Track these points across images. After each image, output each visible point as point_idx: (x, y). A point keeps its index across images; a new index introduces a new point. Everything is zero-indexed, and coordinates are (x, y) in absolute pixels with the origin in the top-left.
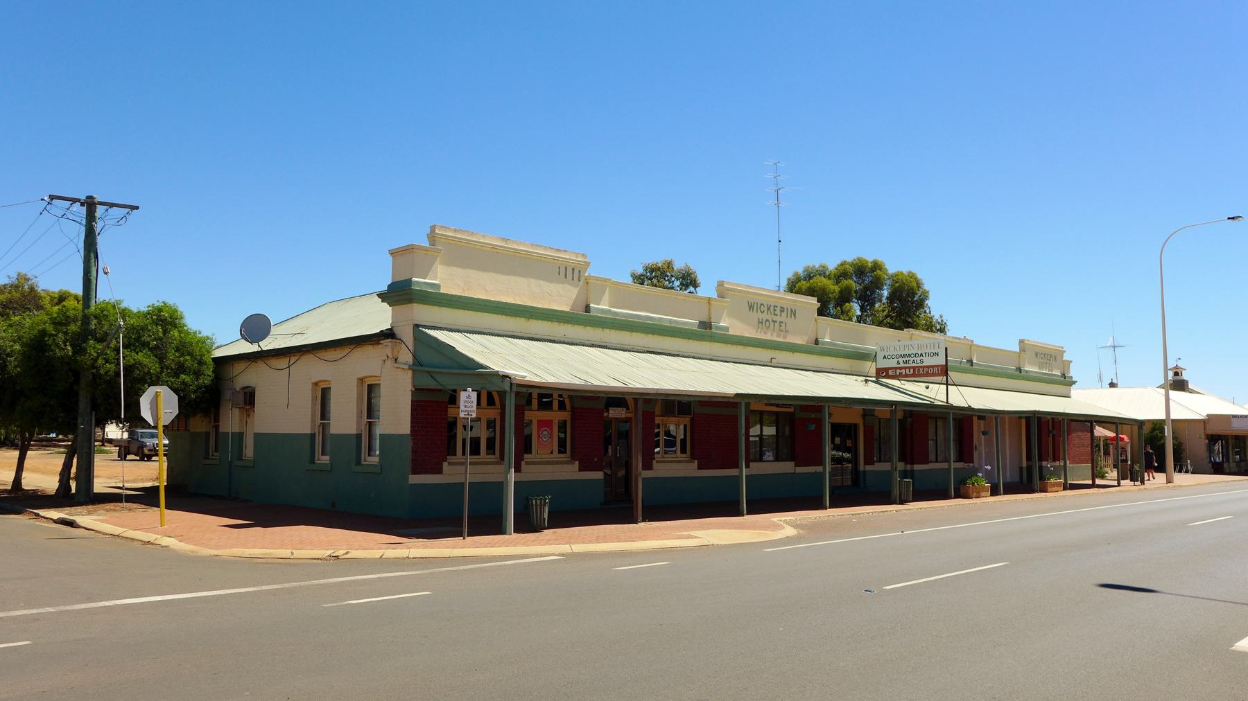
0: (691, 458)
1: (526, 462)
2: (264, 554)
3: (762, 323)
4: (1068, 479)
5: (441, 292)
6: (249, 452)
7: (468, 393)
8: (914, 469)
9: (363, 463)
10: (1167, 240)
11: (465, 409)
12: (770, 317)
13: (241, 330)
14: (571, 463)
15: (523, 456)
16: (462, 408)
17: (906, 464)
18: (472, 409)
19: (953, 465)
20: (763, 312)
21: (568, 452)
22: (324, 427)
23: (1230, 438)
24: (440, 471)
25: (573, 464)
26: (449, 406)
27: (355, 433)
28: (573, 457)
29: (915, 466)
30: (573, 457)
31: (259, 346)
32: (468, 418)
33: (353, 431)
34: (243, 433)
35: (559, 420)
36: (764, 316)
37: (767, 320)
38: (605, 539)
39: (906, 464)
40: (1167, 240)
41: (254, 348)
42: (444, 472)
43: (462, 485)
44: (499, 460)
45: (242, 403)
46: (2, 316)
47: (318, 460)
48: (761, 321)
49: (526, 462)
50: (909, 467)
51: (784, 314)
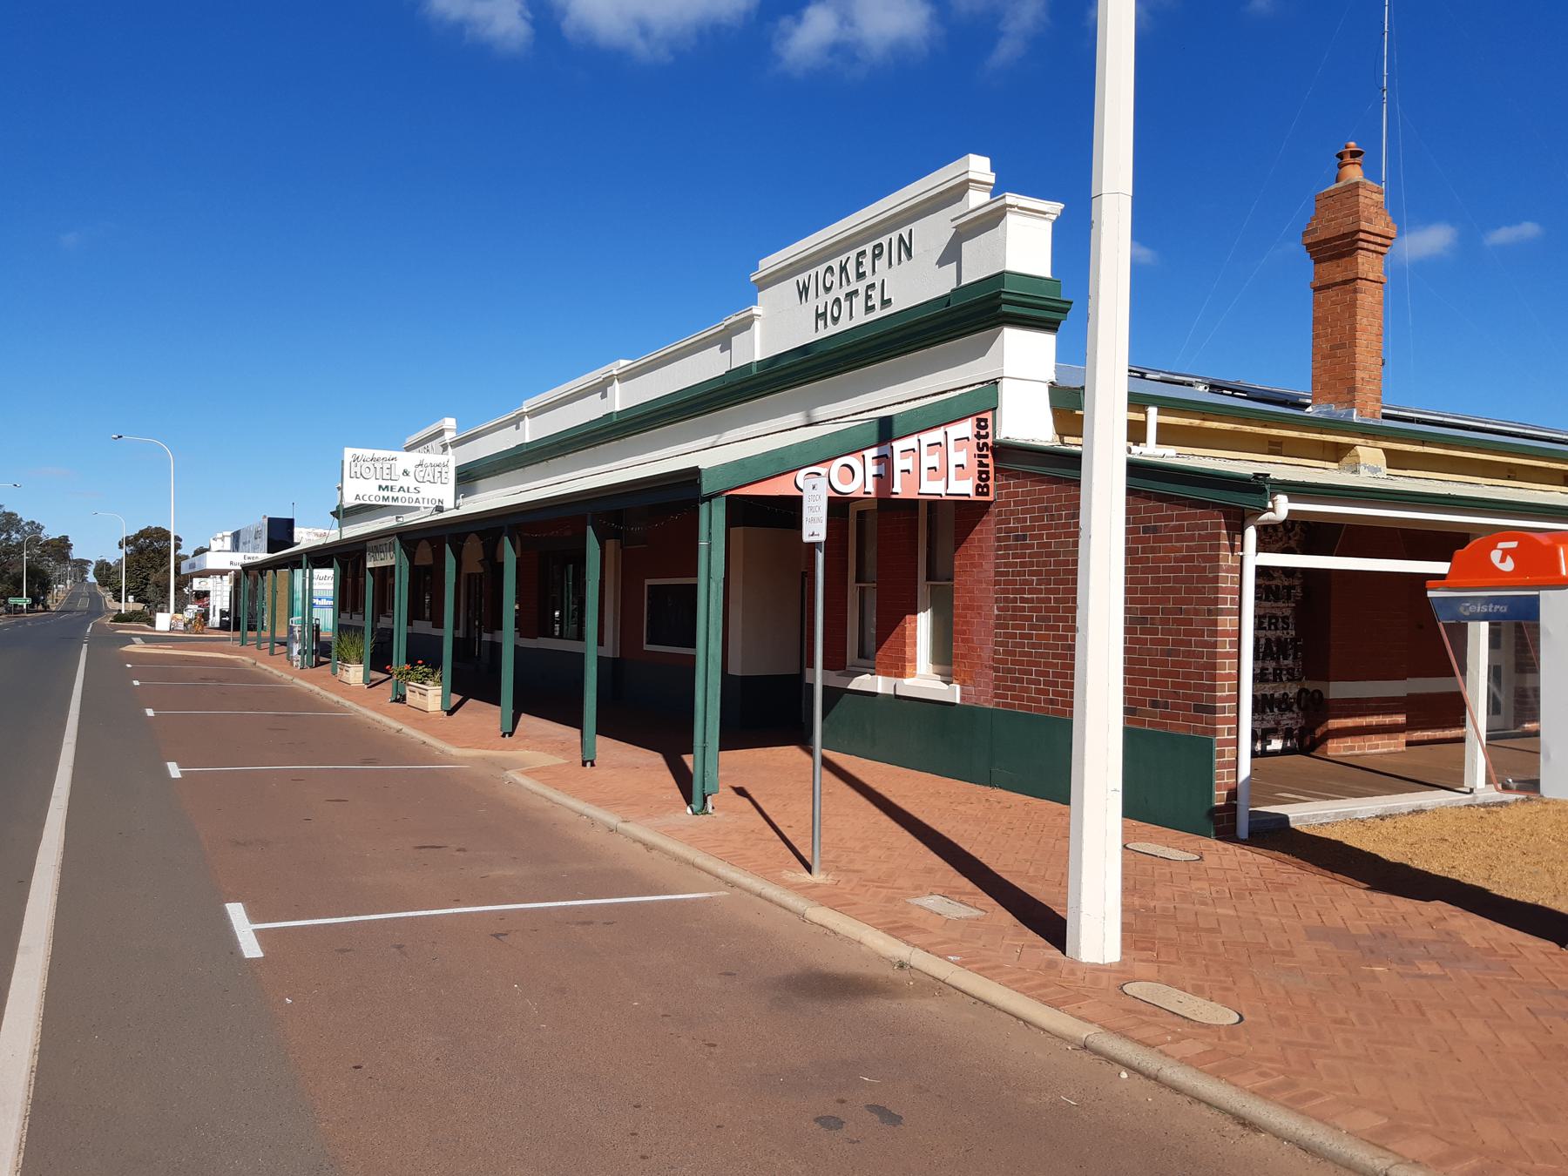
10: (790, 430)
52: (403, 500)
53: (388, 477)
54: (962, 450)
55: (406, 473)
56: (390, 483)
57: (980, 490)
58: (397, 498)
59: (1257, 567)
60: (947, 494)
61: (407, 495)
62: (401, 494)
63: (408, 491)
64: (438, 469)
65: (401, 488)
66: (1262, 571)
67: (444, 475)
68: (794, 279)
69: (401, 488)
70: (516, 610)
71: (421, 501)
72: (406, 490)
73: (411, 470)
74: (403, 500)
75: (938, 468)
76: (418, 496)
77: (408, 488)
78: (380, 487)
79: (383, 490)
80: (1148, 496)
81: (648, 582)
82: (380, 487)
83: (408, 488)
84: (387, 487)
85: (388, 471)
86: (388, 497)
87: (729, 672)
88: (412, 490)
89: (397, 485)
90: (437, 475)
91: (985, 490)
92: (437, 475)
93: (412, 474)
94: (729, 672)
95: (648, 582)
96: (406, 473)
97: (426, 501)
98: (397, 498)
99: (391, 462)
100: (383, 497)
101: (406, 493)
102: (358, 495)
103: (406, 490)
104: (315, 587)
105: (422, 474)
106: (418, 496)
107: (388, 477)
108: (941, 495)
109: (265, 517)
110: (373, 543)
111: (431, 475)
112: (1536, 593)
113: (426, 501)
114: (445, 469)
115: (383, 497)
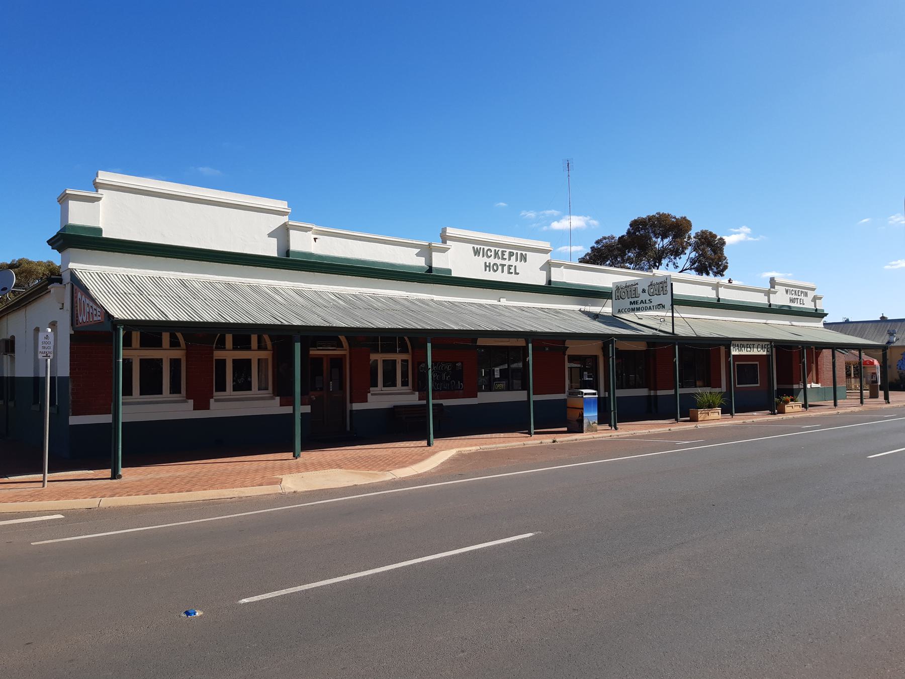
1: (215, 399)
2: (509, 442)
3: (489, 266)
4: (808, 400)
5: (453, 275)
11: (43, 350)
12: (499, 262)
14: (272, 398)
15: (369, 389)
18: (50, 350)
19: (431, 402)
25: (274, 399)
26: (311, 348)
28: (189, 397)
30: (189, 397)
35: (132, 359)
37: (495, 264)
38: (189, 485)
39: (650, 390)
42: (369, 401)
46: (1, 302)
48: (487, 264)
49: (215, 399)
50: (652, 393)
51: (513, 258)
53: (634, 296)
55: (644, 291)
56: (635, 299)
58: (639, 308)
62: (642, 305)
63: (646, 303)
68: (474, 245)
72: (644, 302)
73: (647, 288)
77: (645, 300)
78: (631, 302)
80: (125, 349)
81: (758, 385)
82: (631, 302)
83: (645, 300)
84: (634, 302)
88: (647, 302)
89: (639, 299)
90: (661, 289)
92: (661, 289)
93: (647, 291)
95: (758, 385)
98: (639, 308)
99: (635, 287)
100: (632, 308)
102: (619, 310)
103: (644, 302)
104: (833, 401)
105: (652, 290)
107: (634, 296)
109: (883, 314)
110: (737, 343)
111: (657, 291)
112: (214, 361)
114: (665, 285)
115: (632, 308)
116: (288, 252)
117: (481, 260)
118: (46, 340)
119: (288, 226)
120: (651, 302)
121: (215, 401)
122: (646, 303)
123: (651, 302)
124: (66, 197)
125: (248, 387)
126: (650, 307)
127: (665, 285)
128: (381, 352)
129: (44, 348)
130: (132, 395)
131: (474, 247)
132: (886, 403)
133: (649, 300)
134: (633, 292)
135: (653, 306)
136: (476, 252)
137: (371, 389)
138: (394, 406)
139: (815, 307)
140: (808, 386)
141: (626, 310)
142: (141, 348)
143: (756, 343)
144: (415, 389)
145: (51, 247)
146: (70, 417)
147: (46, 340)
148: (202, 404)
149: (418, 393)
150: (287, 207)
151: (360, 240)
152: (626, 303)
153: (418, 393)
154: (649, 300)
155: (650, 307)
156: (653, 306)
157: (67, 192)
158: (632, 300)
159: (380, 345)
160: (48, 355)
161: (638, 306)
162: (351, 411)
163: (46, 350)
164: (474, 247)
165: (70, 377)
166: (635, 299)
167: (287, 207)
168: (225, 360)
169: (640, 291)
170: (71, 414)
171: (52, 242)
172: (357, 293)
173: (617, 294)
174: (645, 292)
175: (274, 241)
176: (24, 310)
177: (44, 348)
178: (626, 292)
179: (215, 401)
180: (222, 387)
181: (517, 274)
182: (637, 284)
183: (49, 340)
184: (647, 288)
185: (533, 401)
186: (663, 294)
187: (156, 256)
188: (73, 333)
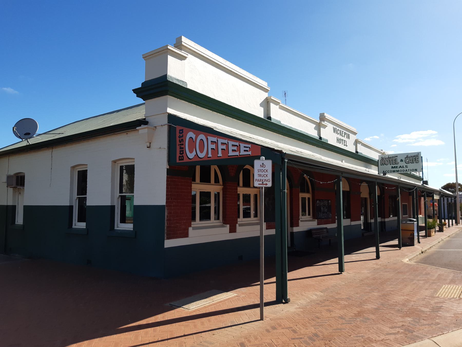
0: (313, 218)
6: (20, 220)
7: (263, 162)
8: (386, 221)
9: (116, 228)
10: (456, 117)
11: (259, 178)
13: (13, 128)
16: (256, 177)
17: (382, 218)
18: (266, 178)
20: (338, 134)
21: (311, 215)
22: (82, 201)
23: (200, 206)
24: (186, 235)
26: (193, 182)
27: (69, 205)
29: (386, 219)
31: (28, 142)
32: (262, 188)
33: (108, 203)
34: (15, 206)
36: (340, 137)
40: (456, 117)
41: (24, 143)
43: (13, 208)
44: (222, 224)
45: (14, 185)
47: (75, 225)
49: (239, 224)
50: (383, 220)
52: (401, 171)
53: (395, 163)
54: (214, 144)
55: (402, 161)
56: (396, 165)
57: (180, 158)
58: (399, 170)
59: (211, 192)
60: (240, 155)
61: (402, 169)
62: (400, 169)
63: (403, 167)
64: (414, 158)
65: (400, 167)
66: (201, 219)
67: (417, 160)
69: (400, 167)
70: (254, 213)
71: (408, 170)
72: (402, 167)
73: (404, 159)
74: (401, 171)
75: (225, 149)
76: (407, 169)
77: (403, 166)
79: (393, 168)
83: (403, 166)
84: (395, 167)
85: (394, 161)
86: (395, 170)
87: (275, 299)
88: (404, 167)
90: (414, 160)
91: (182, 158)
92: (414, 160)
93: (404, 161)
94: (275, 299)
96: (402, 161)
97: (410, 170)
98: (399, 170)
99: (395, 158)
100: (393, 171)
101: (402, 168)
102: (384, 171)
103: (402, 167)
105: (408, 160)
106: (407, 169)
108: (238, 155)
113: (410, 170)
115: (393, 171)
116: (269, 118)
117: (336, 136)
118: (261, 168)
119: (270, 100)
120: (407, 167)
121: (193, 229)
122: (403, 167)
123: (407, 167)
124: (165, 51)
125: (208, 218)
126: (406, 170)
127: (417, 158)
128: (307, 193)
129: (260, 175)
130: (243, 218)
131: (333, 127)
132: (456, 225)
133: (406, 166)
134: (394, 161)
135: (409, 170)
136: (335, 130)
137: (192, 223)
138: (310, 229)
139: (419, 175)
140: (419, 216)
141: (389, 172)
142: (201, 183)
143: (217, 206)
144: (225, 222)
145: (136, 95)
146: (165, 240)
147: (261, 168)
148: (233, 230)
149: (316, 220)
150: (267, 86)
151: (293, 114)
152: (389, 167)
153: (316, 220)
154: (406, 166)
155: (406, 170)
156: (409, 170)
157: (169, 47)
158: (393, 166)
159: (286, 190)
160: (264, 183)
161: (397, 169)
162: (292, 234)
163: (261, 178)
164: (333, 127)
165: (167, 206)
166: (396, 165)
167: (267, 86)
168: (24, 206)
169: (399, 160)
170: (166, 238)
171: (138, 92)
172: (295, 151)
173: (382, 162)
174: (402, 161)
175: (262, 109)
176: (51, 150)
177: (260, 175)
178: (389, 161)
179: (193, 229)
180: (194, 219)
181: (347, 146)
182: (397, 156)
183: (265, 168)
184: (404, 159)
185: (344, 226)
186: (416, 163)
187: (241, 110)
188: (168, 168)
